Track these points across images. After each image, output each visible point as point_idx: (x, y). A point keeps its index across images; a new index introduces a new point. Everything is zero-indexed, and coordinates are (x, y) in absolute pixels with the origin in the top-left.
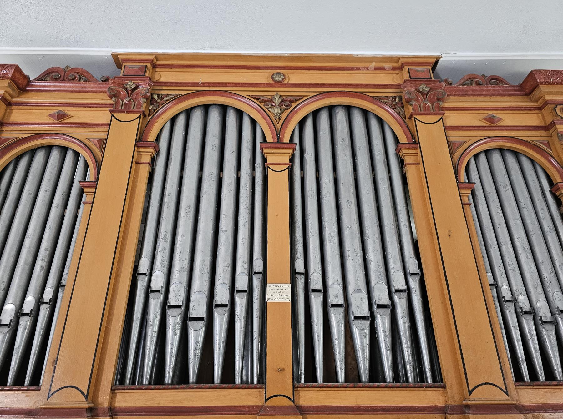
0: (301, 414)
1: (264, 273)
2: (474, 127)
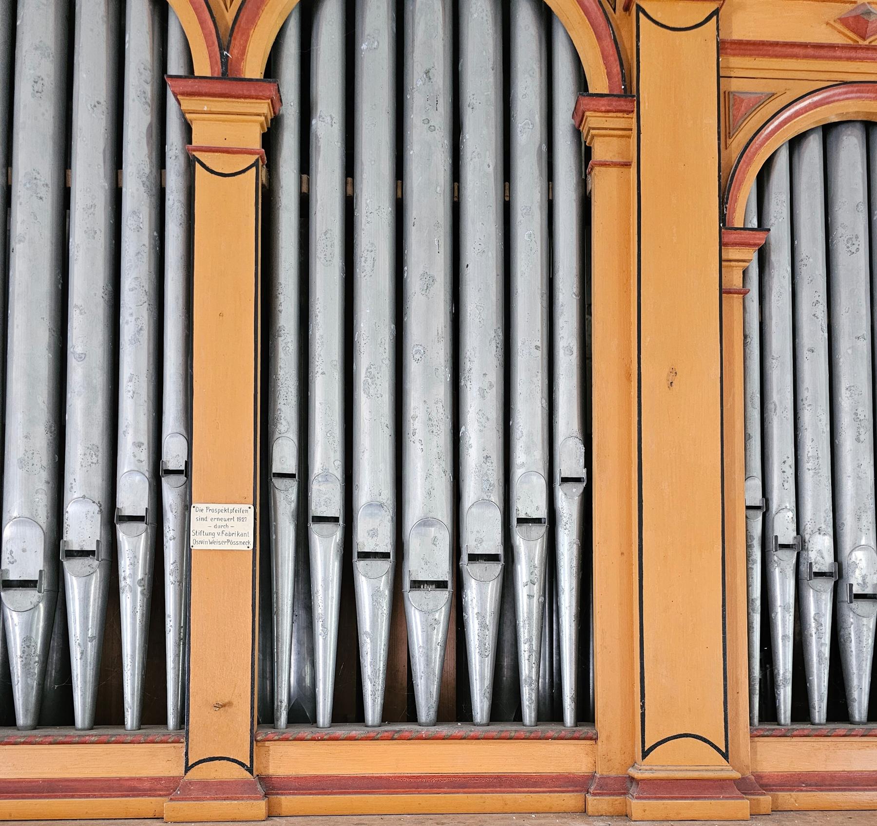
0: (266, 795)
1: (187, 471)
2: (805, 46)
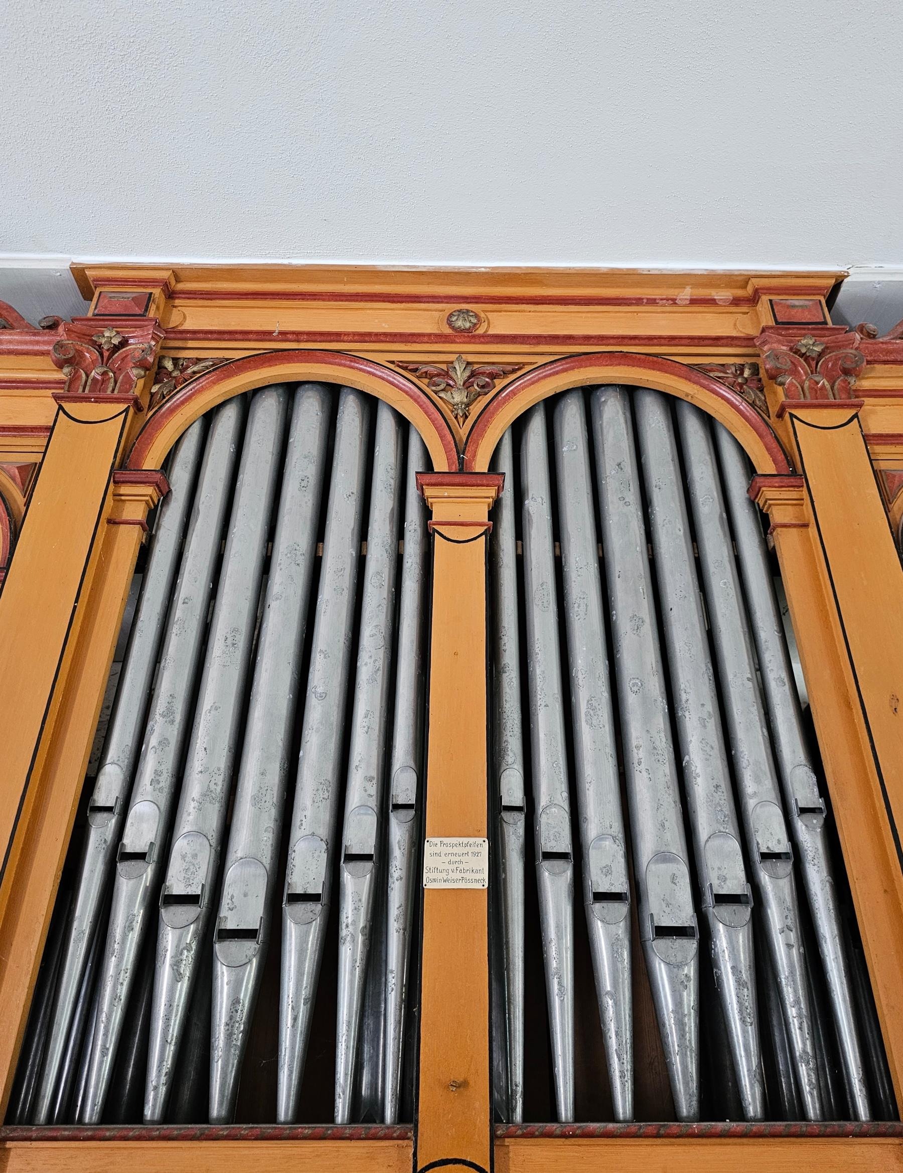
1: (419, 806)
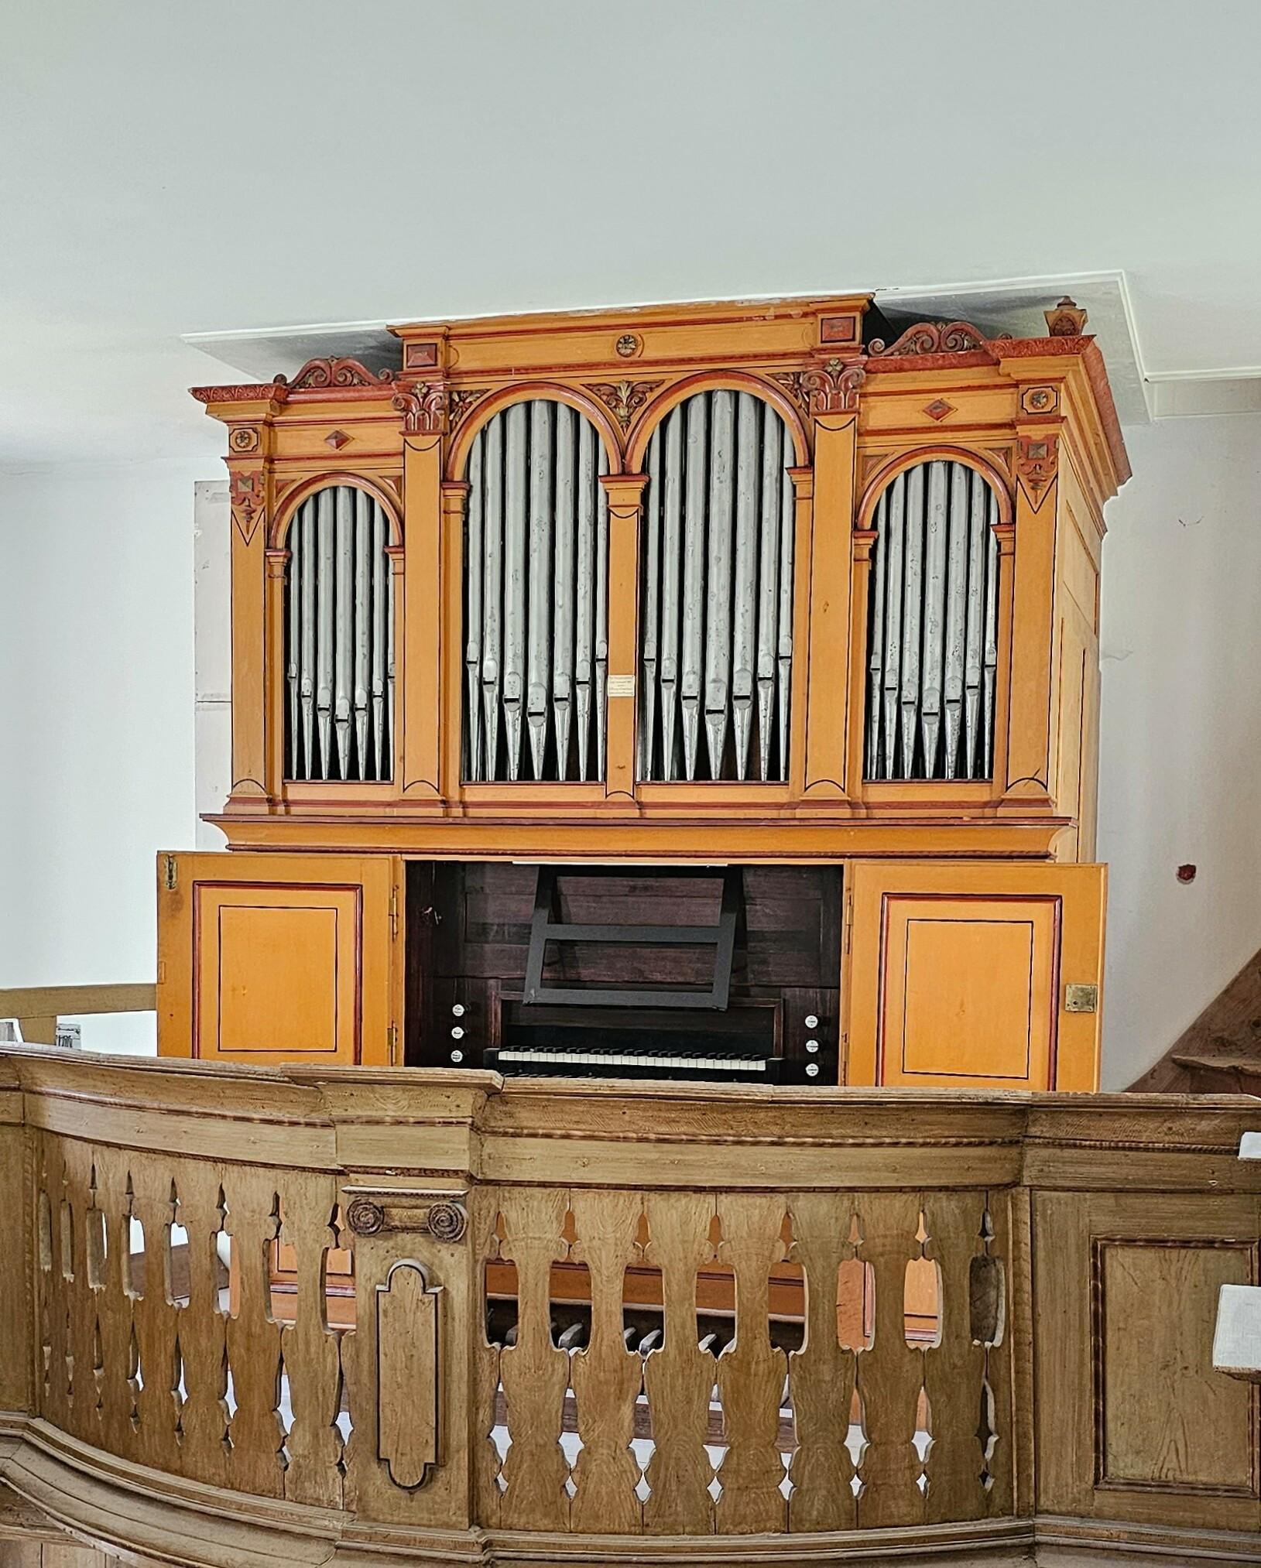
1: (606, 660)
